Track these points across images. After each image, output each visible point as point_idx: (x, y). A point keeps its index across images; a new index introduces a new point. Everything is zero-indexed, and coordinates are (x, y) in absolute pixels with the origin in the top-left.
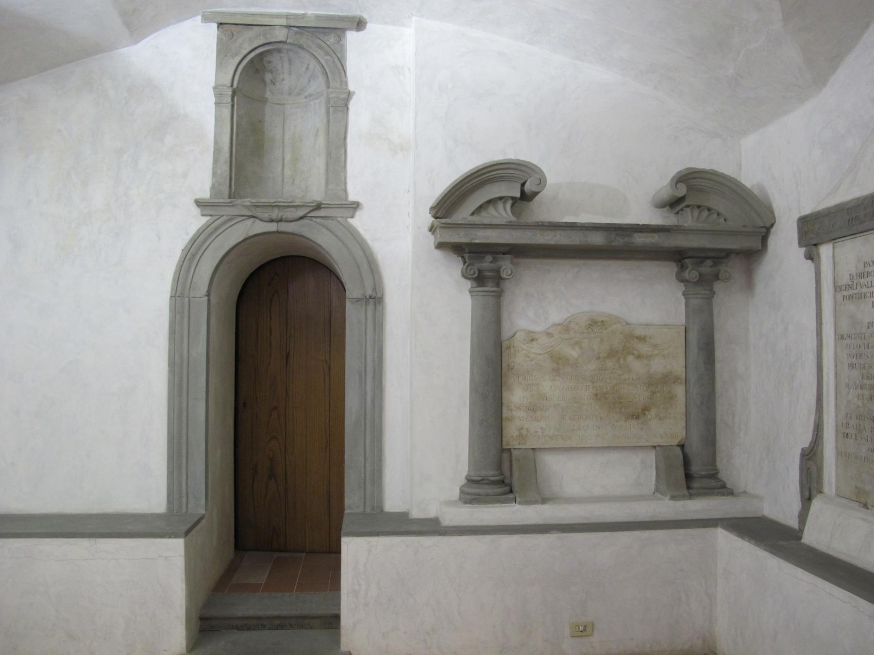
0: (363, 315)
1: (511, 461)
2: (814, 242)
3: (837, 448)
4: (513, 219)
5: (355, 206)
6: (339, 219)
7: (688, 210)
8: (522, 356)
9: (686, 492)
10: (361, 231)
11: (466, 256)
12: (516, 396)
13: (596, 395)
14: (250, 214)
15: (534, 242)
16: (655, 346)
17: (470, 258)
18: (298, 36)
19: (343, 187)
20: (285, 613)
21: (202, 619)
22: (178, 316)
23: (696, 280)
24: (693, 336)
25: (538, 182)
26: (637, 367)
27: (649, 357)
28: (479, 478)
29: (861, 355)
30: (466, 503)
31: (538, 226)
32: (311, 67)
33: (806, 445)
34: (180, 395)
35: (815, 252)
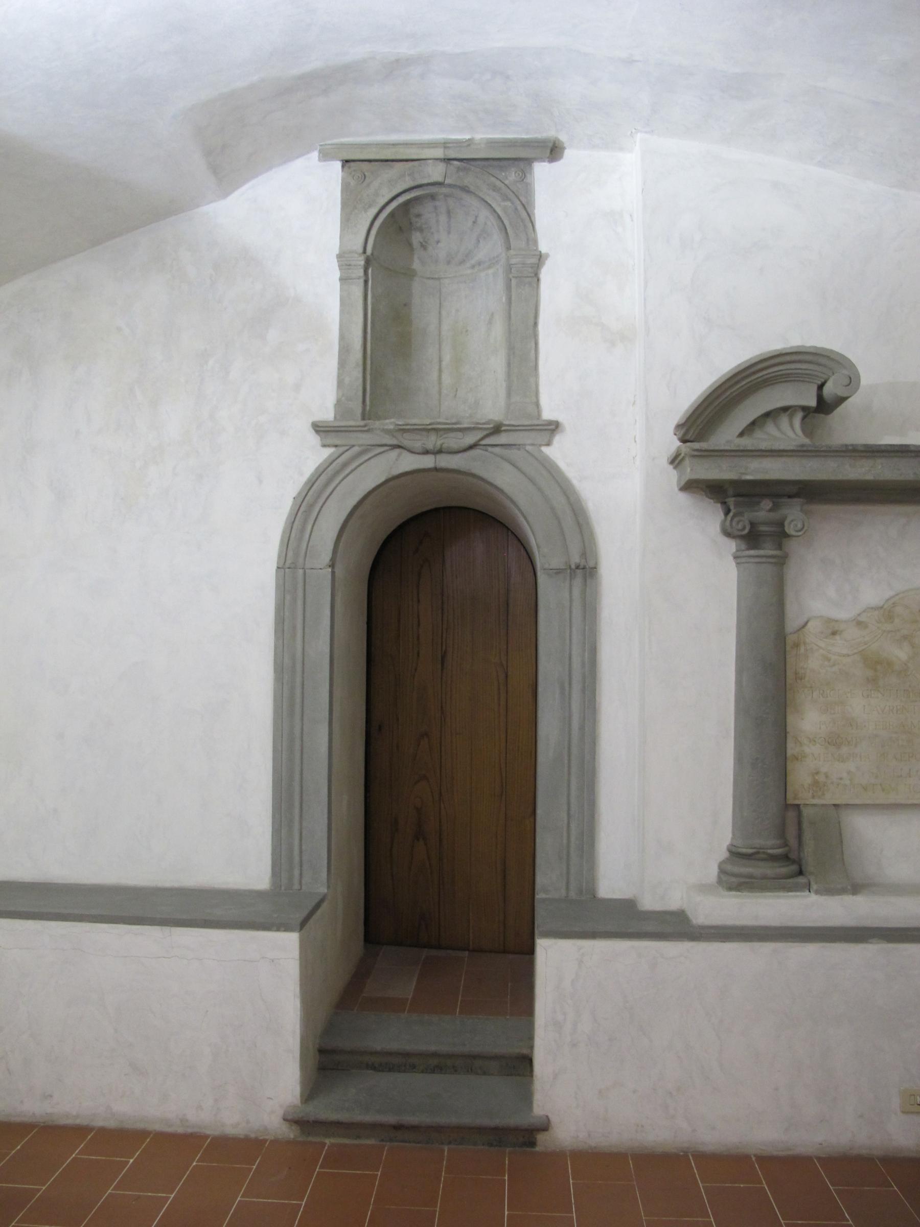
0: (567, 595)
1: (800, 823)
4: (807, 441)
5: (553, 428)
8: (817, 659)
10: (562, 465)
11: (731, 501)
12: (809, 721)
14: (395, 442)
15: (840, 477)
17: (737, 505)
18: (461, 174)
19: (534, 399)
20: (444, 1049)
21: (321, 1051)
22: (288, 597)
25: (847, 381)
28: (750, 851)
30: (730, 889)
32: (481, 219)
34: (291, 714)
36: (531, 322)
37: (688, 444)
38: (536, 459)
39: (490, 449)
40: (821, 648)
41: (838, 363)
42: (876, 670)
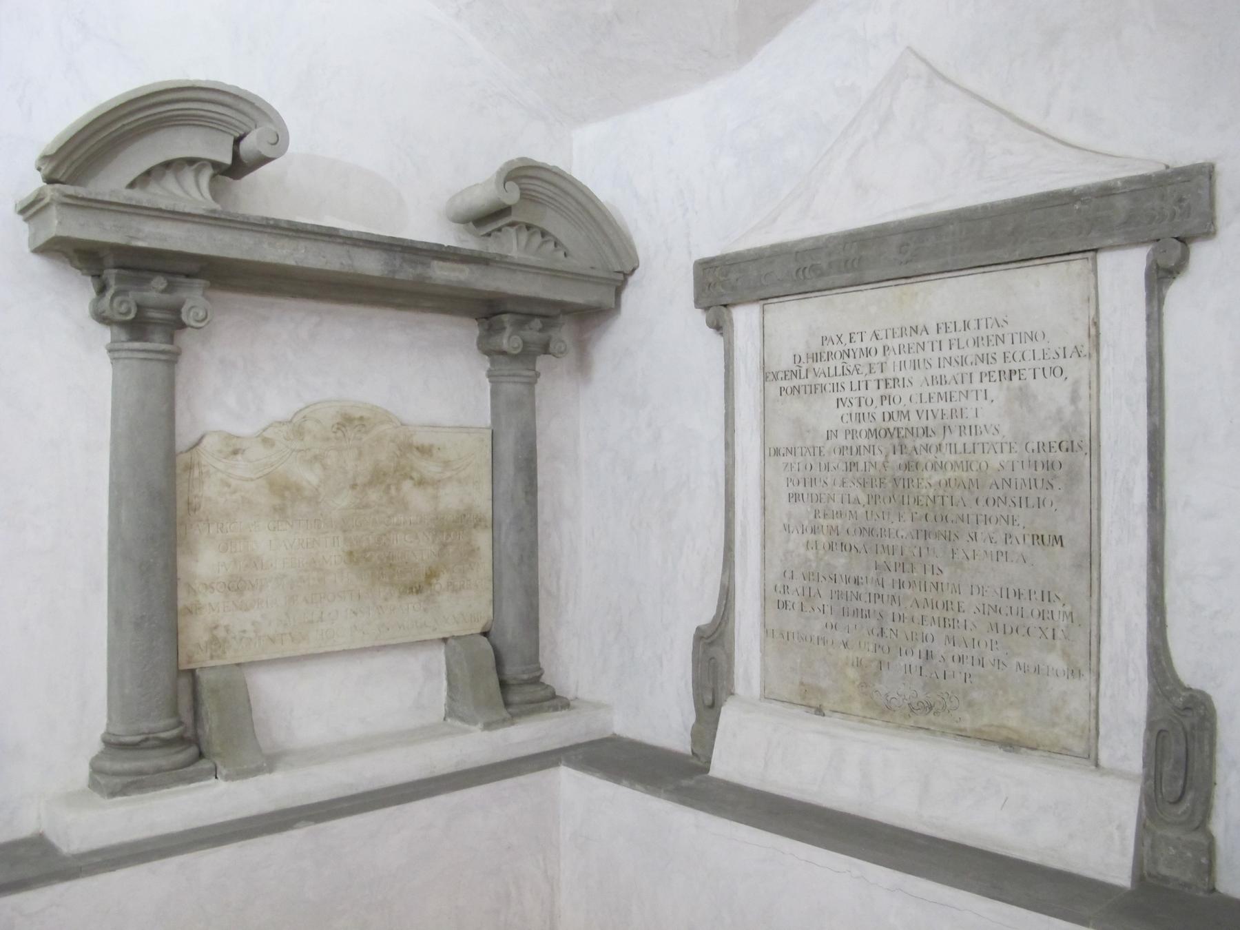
7: (512, 230)
8: (216, 484)
9: (504, 713)
11: (111, 275)
12: (206, 563)
13: (351, 553)
16: (446, 464)
17: (119, 279)
24: (508, 446)
26: (418, 500)
27: (436, 483)
28: (138, 738)
29: (813, 481)
30: (113, 794)
31: (267, 226)
37: (57, 186)
40: (218, 470)
41: (265, 114)
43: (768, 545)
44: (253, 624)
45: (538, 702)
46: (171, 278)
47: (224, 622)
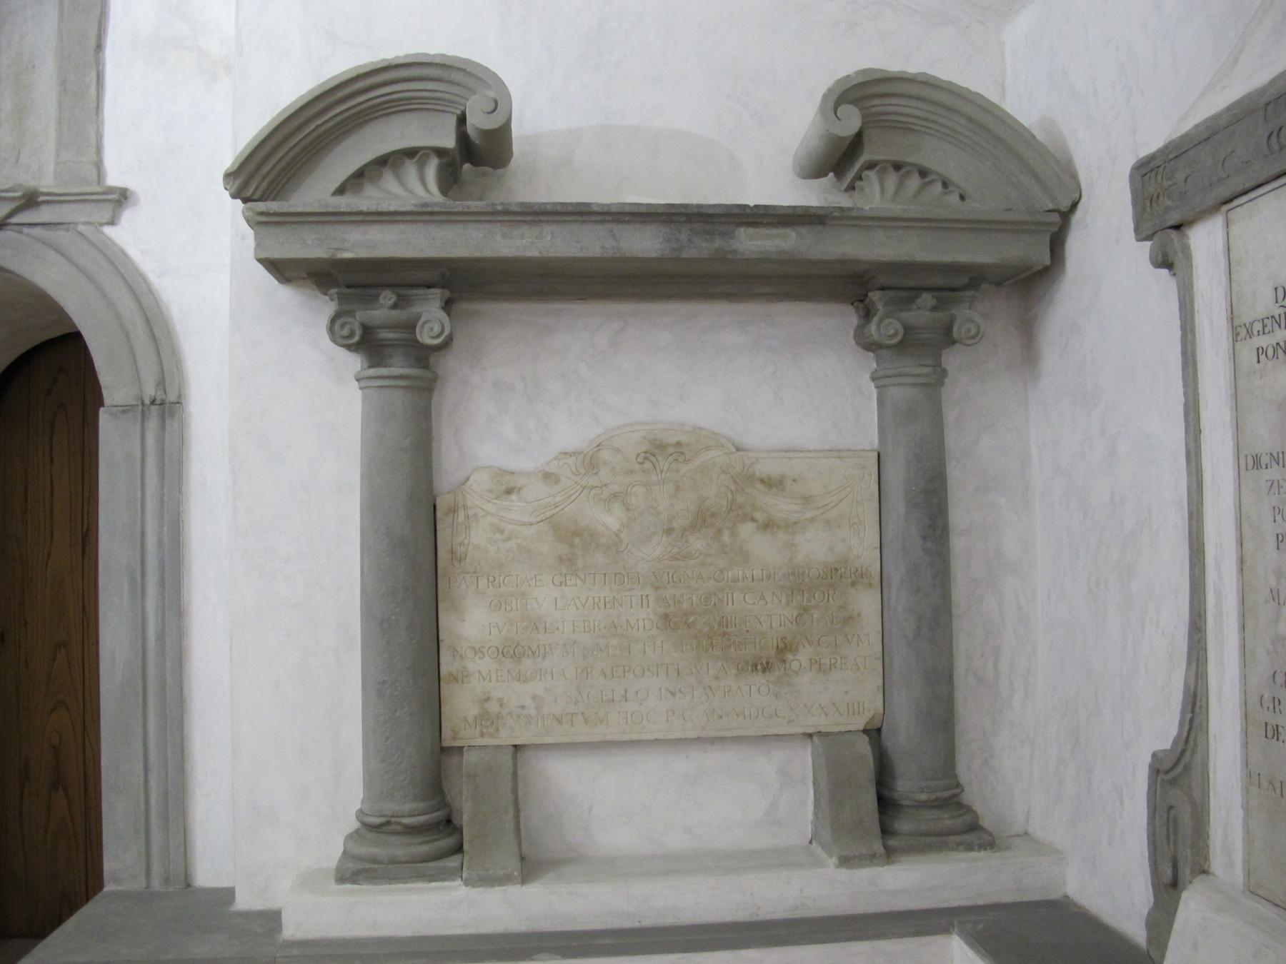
2: (1174, 218)
3: (1246, 763)
5: (122, 198)
6: (81, 228)
7: (872, 175)
9: (878, 846)
12: (472, 623)
13: (666, 616)
15: (488, 253)
16: (806, 500)
19: (93, 157)
23: (895, 341)
24: (896, 476)
25: (490, 107)
26: (765, 550)
27: (791, 526)
28: (378, 821)
33: (1166, 744)
35: (1177, 246)
36: (92, 43)
38: (93, 244)
39: (26, 230)
40: (488, 513)
42: (572, 546)
43: (1249, 624)
44: (534, 698)
45: (940, 835)
46: (403, 292)
47: (497, 694)
